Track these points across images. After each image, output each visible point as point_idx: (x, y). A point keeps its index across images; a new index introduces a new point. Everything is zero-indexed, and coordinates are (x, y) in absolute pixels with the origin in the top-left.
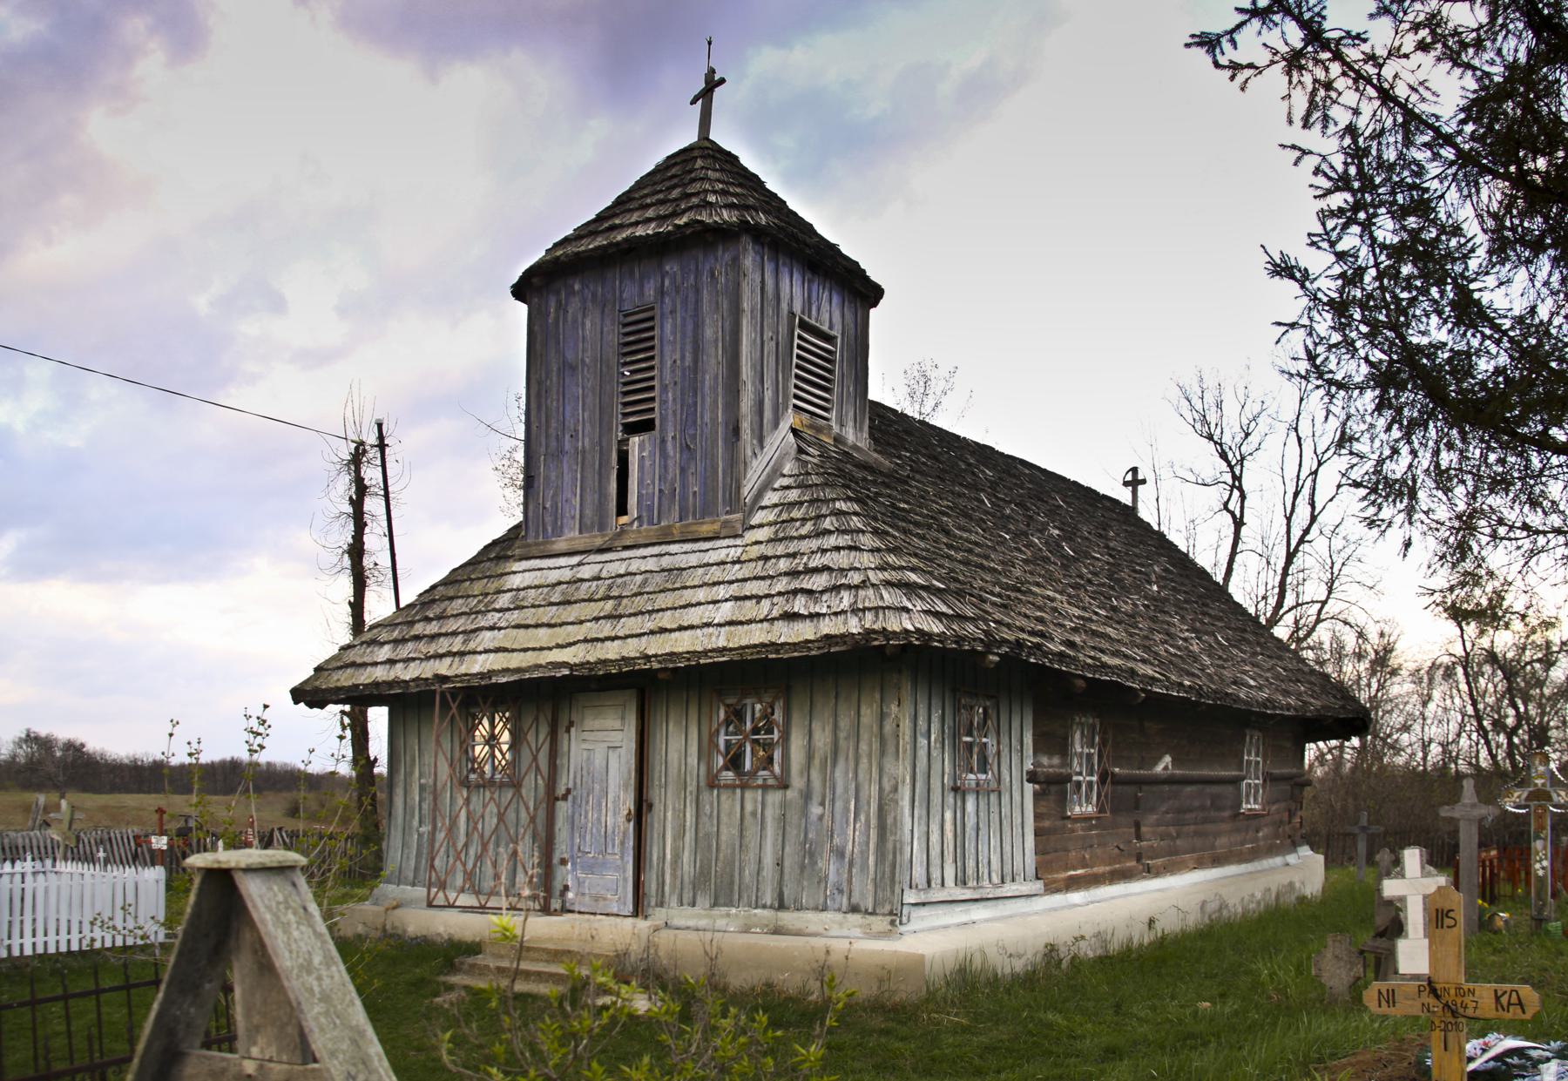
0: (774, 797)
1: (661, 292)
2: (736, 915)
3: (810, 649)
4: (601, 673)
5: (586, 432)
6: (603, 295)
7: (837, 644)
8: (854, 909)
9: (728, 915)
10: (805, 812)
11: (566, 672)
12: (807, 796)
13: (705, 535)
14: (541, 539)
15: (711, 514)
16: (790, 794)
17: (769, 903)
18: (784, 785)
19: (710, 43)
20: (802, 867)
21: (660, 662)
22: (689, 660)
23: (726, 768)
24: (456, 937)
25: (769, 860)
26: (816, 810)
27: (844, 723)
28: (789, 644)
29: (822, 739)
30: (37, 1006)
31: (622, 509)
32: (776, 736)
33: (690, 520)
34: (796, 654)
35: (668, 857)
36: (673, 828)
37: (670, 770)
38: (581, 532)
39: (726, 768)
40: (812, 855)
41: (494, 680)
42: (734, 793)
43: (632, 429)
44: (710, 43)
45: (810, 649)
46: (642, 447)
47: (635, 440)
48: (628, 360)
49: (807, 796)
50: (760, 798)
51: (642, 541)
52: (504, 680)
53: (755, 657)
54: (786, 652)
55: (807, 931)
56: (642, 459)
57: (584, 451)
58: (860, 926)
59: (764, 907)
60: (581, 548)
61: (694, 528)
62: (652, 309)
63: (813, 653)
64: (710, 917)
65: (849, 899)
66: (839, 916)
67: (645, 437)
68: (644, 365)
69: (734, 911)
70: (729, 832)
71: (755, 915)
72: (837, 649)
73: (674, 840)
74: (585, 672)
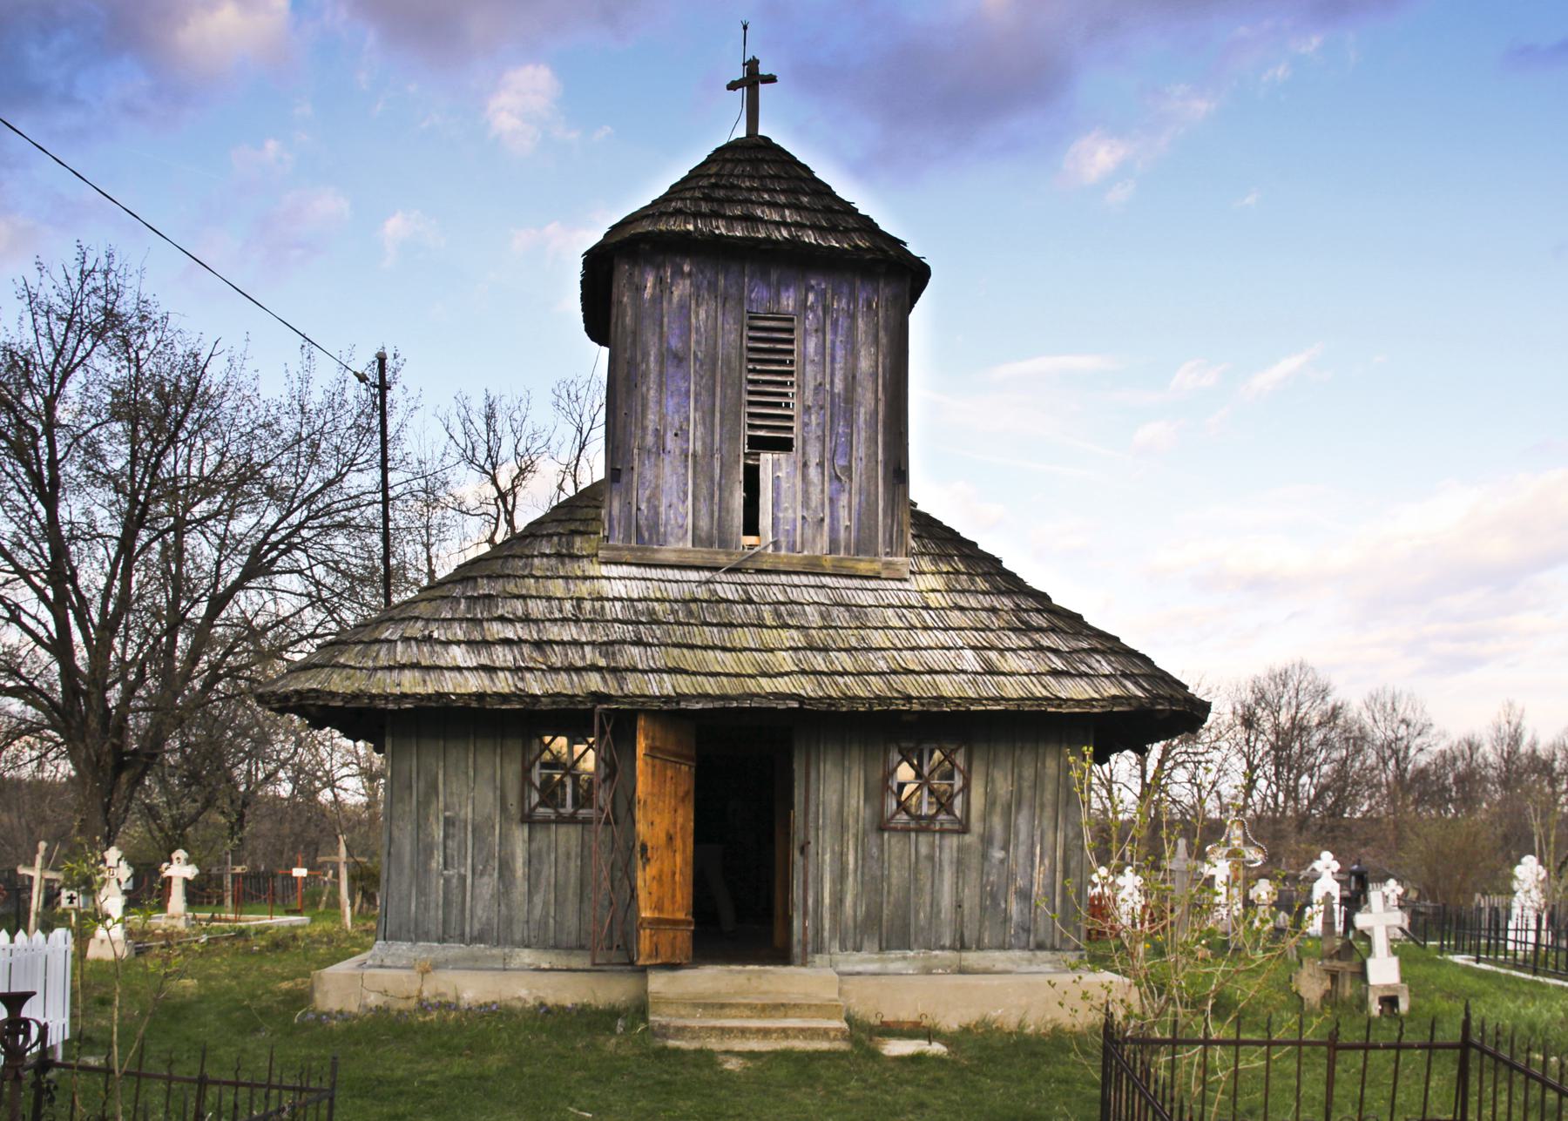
0: (952, 842)
1: (803, 306)
2: (914, 957)
3: (1093, 706)
4: (844, 709)
5: (698, 434)
6: (726, 288)
7: (1121, 704)
8: (1040, 946)
9: (905, 958)
10: (985, 856)
11: (796, 705)
12: (987, 840)
13: (863, 573)
14: (633, 543)
15: (866, 552)
16: (968, 838)
17: (948, 944)
18: (964, 829)
19: (745, 28)
20: (983, 908)
21: (923, 705)
22: (958, 705)
23: (542, 803)
24: (482, 1002)
25: (946, 900)
26: (998, 854)
27: (1028, 772)
28: (1072, 700)
29: (1003, 787)
30: (1242, 1048)
31: (751, 527)
32: (958, 782)
33: (842, 555)
34: (1077, 710)
35: (827, 901)
36: (831, 871)
37: (828, 812)
38: (694, 545)
39: (542, 803)
40: (993, 896)
41: (683, 705)
42: (549, 829)
43: (758, 444)
44: (745, 28)
45: (1093, 706)
46: (776, 465)
47: (766, 459)
48: (758, 367)
49: (987, 840)
50: (937, 842)
51: (782, 567)
52: (699, 706)
53: (1035, 708)
54: (1069, 707)
55: (995, 969)
56: (776, 480)
57: (695, 455)
58: (1050, 962)
59: (943, 948)
60: (698, 562)
61: (849, 564)
62: (792, 320)
63: (1096, 710)
64: (882, 960)
65: (1035, 936)
66: (1027, 954)
67: (782, 456)
68: (779, 378)
69: (911, 954)
70: (897, 877)
71: (936, 956)
72: (1121, 709)
73: (833, 882)
74: (823, 707)
